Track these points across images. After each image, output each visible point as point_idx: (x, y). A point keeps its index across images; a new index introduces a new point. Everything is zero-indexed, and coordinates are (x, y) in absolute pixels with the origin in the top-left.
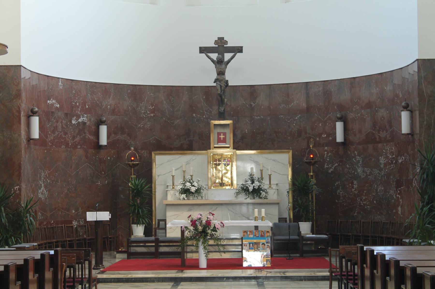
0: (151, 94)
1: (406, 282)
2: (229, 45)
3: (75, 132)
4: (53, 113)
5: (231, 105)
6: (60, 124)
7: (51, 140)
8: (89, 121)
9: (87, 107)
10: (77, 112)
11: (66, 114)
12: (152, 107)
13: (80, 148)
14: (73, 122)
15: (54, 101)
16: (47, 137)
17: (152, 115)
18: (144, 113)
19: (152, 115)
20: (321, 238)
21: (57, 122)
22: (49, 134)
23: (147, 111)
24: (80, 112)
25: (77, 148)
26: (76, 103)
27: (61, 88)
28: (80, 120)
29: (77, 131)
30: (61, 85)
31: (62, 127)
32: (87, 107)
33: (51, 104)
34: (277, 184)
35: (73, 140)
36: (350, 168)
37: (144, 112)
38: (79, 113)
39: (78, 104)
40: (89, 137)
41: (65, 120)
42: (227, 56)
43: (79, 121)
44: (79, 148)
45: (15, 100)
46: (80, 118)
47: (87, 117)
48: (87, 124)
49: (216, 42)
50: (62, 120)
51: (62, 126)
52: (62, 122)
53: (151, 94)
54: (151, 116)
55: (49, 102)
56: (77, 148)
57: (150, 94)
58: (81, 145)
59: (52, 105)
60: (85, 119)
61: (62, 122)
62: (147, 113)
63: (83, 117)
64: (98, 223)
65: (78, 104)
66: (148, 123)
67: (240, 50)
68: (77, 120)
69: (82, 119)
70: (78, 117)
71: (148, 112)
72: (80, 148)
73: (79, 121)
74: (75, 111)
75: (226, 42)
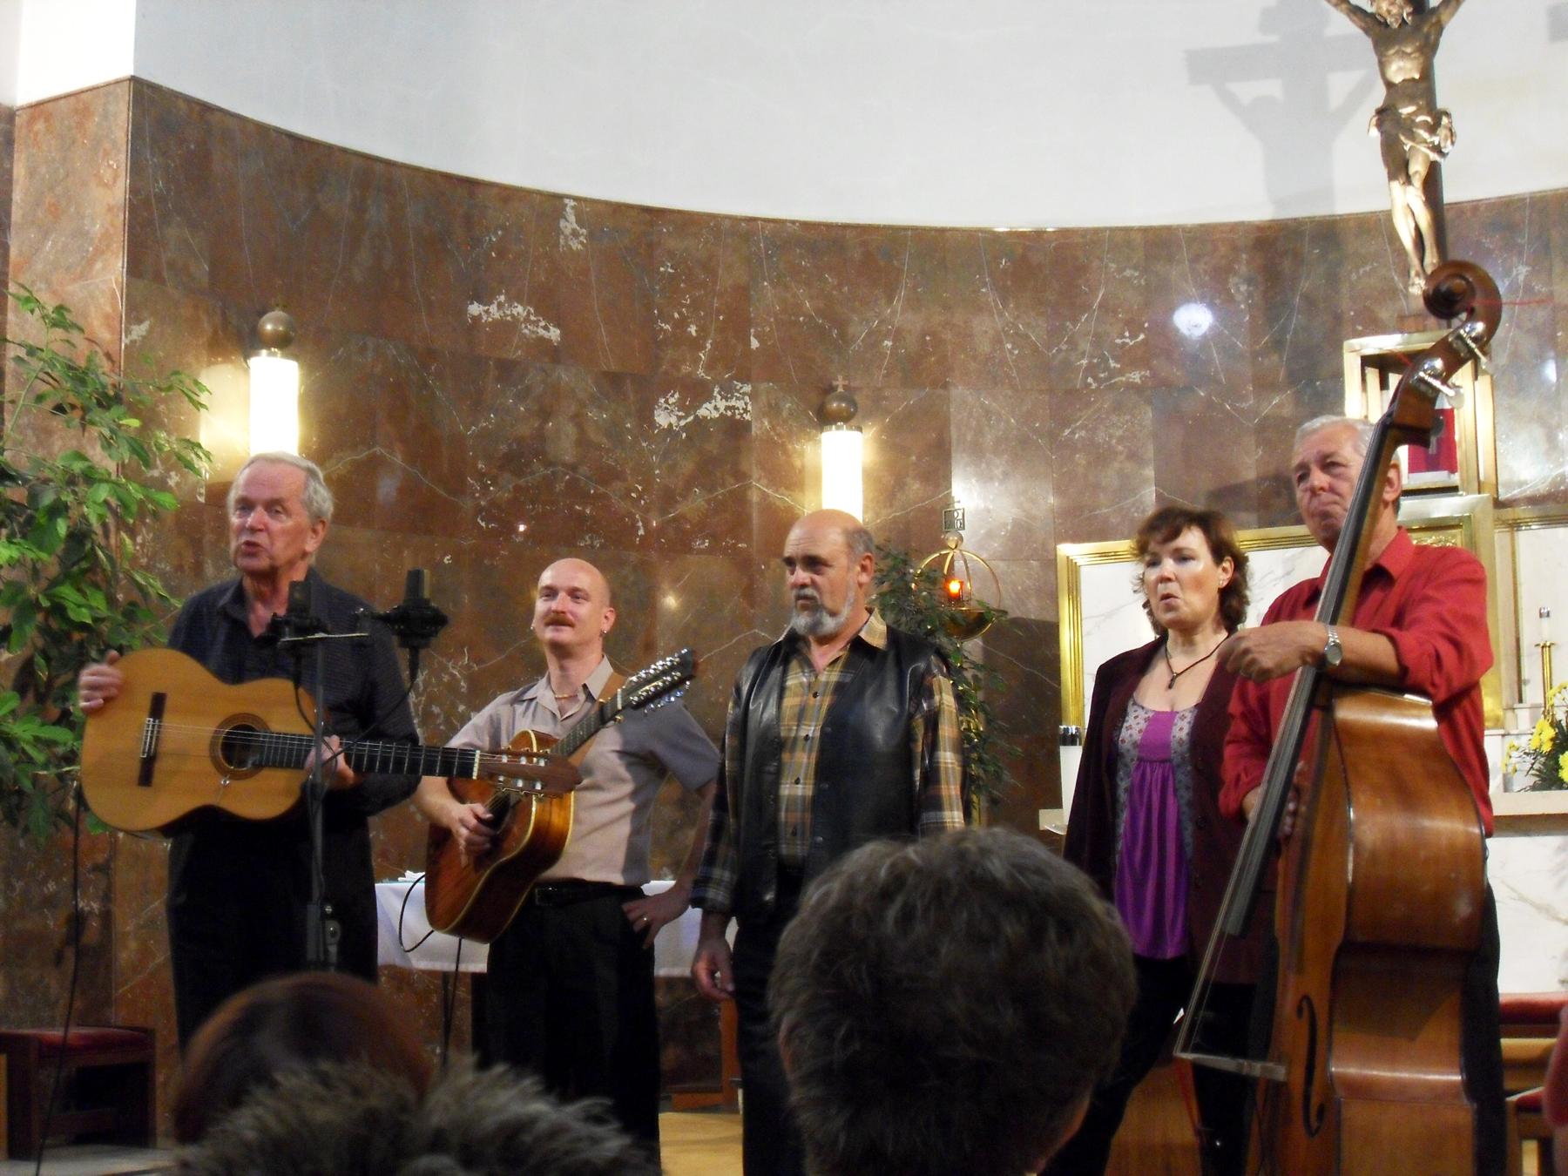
0: (1128, 273)
3: (672, 469)
4: (507, 370)
6: (570, 429)
7: (492, 503)
9: (755, 344)
12: (1133, 336)
13: (710, 551)
14: (663, 419)
17: (1135, 377)
18: (1091, 370)
19: (1135, 377)
20: (1217, 1066)
21: (545, 414)
22: (480, 476)
23: (1104, 360)
24: (710, 367)
25: (690, 550)
26: (682, 324)
28: (706, 411)
29: (687, 466)
30: (575, 234)
31: (582, 442)
33: (499, 325)
34: (1541, 615)
35: (664, 511)
38: (701, 373)
40: (765, 496)
41: (601, 408)
43: (702, 412)
44: (700, 552)
45: (99, 265)
46: (710, 398)
47: (753, 396)
48: (755, 430)
52: (578, 419)
53: (1128, 273)
54: (1131, 386)
55: (475, 309)
56: (690, 550)
58: (714, 537)
59: (507, 328)
60: (740, 404)
61: (578, 419)
62: (1107, 368)
63: (728, 392)
64: (739, 936)
65: (693, 330)
66: (1114, 418)
68: (687, 408)
69: (722, 404)
70: (697, 393)
71: (1112, 364)
72: (710, 551)
73: (702, 412)
74: (675, 365)
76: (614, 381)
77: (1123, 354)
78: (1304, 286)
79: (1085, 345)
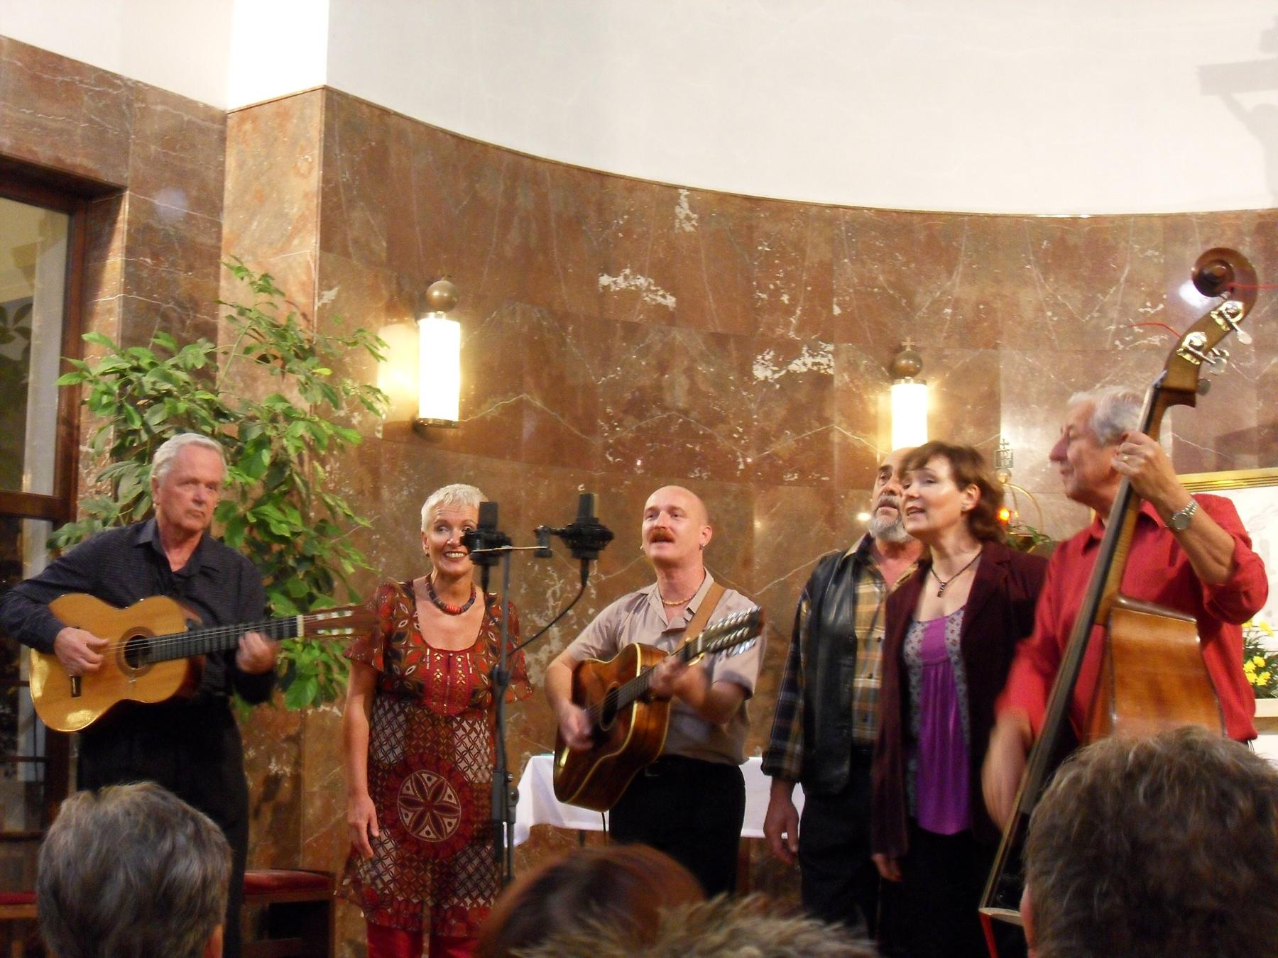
0: (1149, 253)
1: (1200, 316)
3: (767, 415)
6: (683, 381)
9: (837, 311)
10: (780, 331)
11: (719, 341)
12: (1154, 306)
16: (591, 429)
18: (1118, 334)
21: (663, 368)
22: (608, 419)
24: (799, 330)
25: (782, 482)
26: (776, 293)
27: (688, 228)
28: (797, 366)
29: (780, 412)
30: (688, 218)
31: (693, 391)
32: (837, 311)
37: (1118, 330)
40: (845, 437)
41: (709, 363)
43: (793, 367)
44: (790, 483)
45: (296, 242)
47: (835, 354)
50: (694, 361)
51: (693, 383)
52: (690, 372)
53: (1149, 253)
55: (605, 280)
56: (782, 482)
57: (1143, 251)
58: (802, 472)
59: (632, 296)
60: (824, 361)
61: (690, 372)
62: (1132, 333)
63: (814, 351)
65: (785, 298)
68: (780, 363)
69: (809, 361)
70: (788, 351)
73: (793, 367)
74: (771, 328)
76: (719, 341)
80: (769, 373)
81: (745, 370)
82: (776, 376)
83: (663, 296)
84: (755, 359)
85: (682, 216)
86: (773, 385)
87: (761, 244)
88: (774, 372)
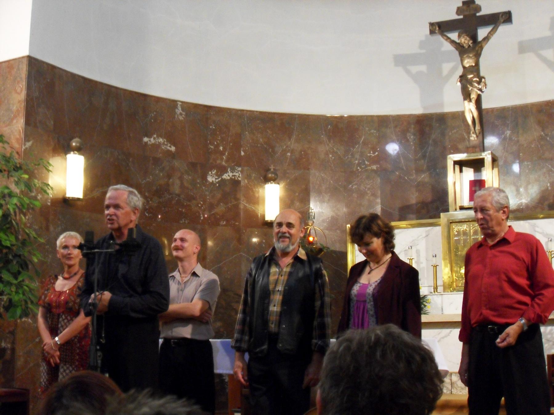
0: (372, 131)
2: (483, 12)
5: (518, 141)
6: (178, 182)
8: (246, 178)
9: (242, 153)
10: (218, 162)
14: (210, 179)
15: (161, 140)
17: (374, 167)
18: (359, 164)
19: (374, 167)
21: (169, 176)
23: (364, 161)
25: (219, 225)
26: (217, 146)
27: (181, 118)
28: (226, 176)
29: (219, 196)
30: (181, 114)
32: (242, 153)
33: (153, 145)
36: (210, 143)
39: (221, 148)
40: (245, 206)
41: (189, 175)
42: (482, 33)
46: (227, 172)
47: (242, 172)
49: (459, 11)
52: (181, 178)
53: (372, 131)
55: (146, 139)
56: (219, 225)
57: (370, 130)
58: (227, 221)
60: (237, 174)
61: (181, 178)
62: (364, 164)
63: (233, 170)
65: (221, 148)
66: (367, 181)
67: (507, 17)
68: (219, 174)
69: (231, 174)
70: (222, 170)
71: (366, 163)
75: (479, 9)
76: (193, 165)
77: (370, 159)
78: (433, 137)
79: (357, 156)
80: (214, 179)
81: (204, 178)
82: (217, 181)
83: (170, 147)
84: (208, 173)
85: (178, 113)
86: (216, 184)
87: (211, 125)
88: (216, 179)
